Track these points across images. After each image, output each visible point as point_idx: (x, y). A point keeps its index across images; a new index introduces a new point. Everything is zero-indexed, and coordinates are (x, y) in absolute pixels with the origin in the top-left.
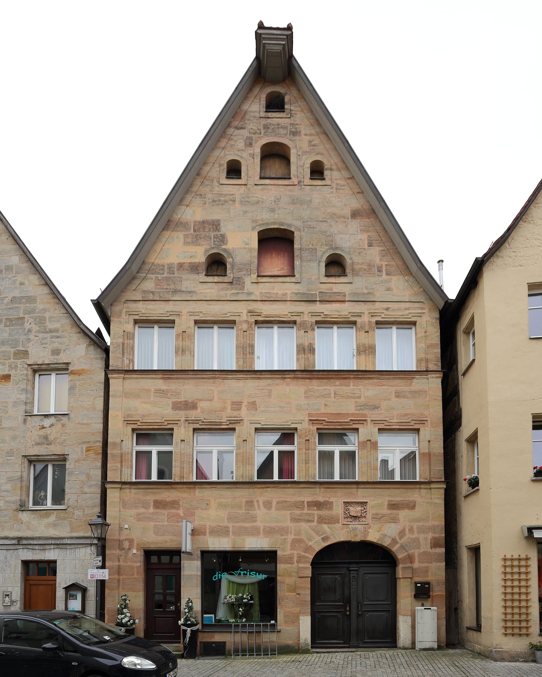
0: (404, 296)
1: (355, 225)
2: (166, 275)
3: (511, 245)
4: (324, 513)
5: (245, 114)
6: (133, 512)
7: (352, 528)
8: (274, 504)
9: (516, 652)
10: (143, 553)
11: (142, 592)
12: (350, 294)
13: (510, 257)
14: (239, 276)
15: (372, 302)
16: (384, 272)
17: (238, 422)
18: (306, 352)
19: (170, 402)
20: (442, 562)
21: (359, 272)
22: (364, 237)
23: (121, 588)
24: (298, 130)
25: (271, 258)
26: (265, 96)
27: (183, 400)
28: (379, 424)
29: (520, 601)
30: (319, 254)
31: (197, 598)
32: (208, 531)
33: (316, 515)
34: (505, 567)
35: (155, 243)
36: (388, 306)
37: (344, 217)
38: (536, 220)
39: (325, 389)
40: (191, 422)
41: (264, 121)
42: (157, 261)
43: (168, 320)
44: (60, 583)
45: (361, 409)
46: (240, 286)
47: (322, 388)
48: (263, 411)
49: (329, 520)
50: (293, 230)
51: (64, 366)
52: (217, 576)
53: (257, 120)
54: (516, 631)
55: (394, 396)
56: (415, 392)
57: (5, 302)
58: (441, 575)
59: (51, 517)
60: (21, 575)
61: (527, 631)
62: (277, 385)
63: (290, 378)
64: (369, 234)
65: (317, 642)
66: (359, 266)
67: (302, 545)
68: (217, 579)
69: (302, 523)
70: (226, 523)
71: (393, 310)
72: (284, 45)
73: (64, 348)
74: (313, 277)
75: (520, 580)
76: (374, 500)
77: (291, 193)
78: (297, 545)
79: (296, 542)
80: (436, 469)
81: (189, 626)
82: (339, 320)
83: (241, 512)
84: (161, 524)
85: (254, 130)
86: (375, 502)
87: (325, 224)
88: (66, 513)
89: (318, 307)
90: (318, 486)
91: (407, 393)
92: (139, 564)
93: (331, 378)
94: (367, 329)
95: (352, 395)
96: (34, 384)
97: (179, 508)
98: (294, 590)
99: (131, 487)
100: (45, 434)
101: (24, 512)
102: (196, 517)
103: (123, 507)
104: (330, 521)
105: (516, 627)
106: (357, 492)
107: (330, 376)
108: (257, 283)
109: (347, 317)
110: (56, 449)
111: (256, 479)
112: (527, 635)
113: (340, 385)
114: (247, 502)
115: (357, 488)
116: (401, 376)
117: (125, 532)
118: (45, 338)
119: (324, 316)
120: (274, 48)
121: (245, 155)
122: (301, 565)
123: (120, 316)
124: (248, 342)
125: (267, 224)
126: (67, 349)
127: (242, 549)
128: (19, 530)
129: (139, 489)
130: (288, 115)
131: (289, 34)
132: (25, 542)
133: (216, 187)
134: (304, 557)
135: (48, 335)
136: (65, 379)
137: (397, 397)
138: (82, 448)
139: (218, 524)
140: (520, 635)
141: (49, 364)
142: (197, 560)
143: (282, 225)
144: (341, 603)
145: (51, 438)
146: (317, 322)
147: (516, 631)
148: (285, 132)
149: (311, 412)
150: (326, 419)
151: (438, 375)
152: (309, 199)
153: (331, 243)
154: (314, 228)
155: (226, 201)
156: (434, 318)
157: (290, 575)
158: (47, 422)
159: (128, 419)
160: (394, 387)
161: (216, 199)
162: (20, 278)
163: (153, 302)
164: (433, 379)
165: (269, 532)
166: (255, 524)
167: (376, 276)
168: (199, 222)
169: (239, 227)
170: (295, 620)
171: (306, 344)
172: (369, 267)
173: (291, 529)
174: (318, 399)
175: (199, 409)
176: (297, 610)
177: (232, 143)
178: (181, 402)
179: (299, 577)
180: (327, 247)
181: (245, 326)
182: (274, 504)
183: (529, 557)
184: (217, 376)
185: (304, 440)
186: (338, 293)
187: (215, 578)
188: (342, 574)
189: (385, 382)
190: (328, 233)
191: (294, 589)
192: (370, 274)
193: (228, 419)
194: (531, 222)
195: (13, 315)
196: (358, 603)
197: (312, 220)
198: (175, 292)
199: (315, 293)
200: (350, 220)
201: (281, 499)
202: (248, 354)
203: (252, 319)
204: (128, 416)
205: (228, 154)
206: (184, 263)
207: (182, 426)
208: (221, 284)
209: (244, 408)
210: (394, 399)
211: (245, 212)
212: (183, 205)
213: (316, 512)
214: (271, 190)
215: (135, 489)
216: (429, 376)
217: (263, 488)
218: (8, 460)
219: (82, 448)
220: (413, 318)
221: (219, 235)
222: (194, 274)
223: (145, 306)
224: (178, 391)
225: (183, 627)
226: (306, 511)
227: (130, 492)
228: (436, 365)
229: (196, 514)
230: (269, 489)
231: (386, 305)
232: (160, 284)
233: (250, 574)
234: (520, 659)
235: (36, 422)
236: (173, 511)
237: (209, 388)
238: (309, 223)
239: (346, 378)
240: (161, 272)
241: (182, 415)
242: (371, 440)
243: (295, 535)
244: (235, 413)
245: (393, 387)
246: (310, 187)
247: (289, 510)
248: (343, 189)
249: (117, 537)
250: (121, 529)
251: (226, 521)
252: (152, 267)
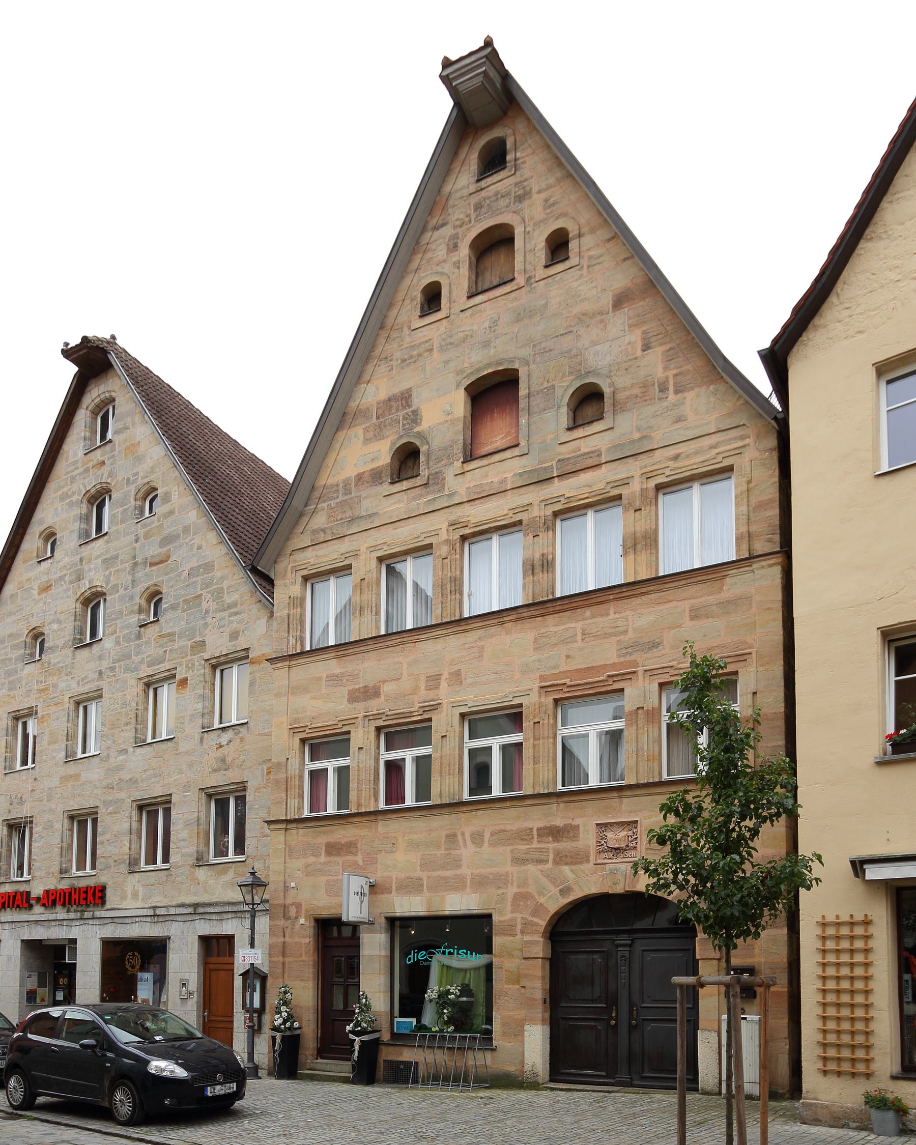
0: (708, 423)
1: (619, 320)
2: (341, 498)
3: (841, 297)
4: (565, 845)
5: (447, 199)
6: (299, 863)
7: (610, 869)
8: (487, 836)
9: (842, 1108)
10: (313, 924)
11: (311, 982)
12: (609, 449)
13: (839, 322)
14: (437, 470)
15: (648, 453)
16: (671, 389)
17: (435, 707)
18: (536, 571)
19: (345, 691)
20: (781, 927)
21: (626, 402)
22: (636, 337)
23: (286, 975)
24: (528, 189)
25: (492, 421)
26: (476, 155)
27: (362, 685)
28: (659, 676)
29: (852, 1006)
30: (559, 392)
31: (380, 992)
32: (394, 887)
33: (551, 851)
34: (824, 938)
35: (327, 454)
36: (677, 451)
37: (601, 313)
38: (891, 229)
39: (567, 629)
40: (371, 718)
41: (474, 199)
42: (332, 481)
43: (344, 566)
44: (238, 968)
45: (627, 653)
46: (439, 486)
47: (562, 627)
48: (470, 684)
49: (572, 857)
50: (516, 367)
51: (243, 654)
52: (411, 956)
53: (465, 201)
54: (846, 1067)
55: (688, 618)
56: (728, 602)
57: (182, 578)
58: (778, 954)
59: (229, 873)
60: (199, 957)
61: (868, 1067)
62: (492, 636)
63: (511, 621)
64: (644, 328)
65: (562, 1071)
66: (627, 393)
67: (529, 902)
68: (412, 961)
69: (529, 865)
70: (418, 873)
71: (688, 456)
72: (485, 72)
73: (243, 628)
74: (550, 437)
75: (852, 965)
76: (650, 817)
77: (515, 304)
78: (522, 903)
79: (521, 898)
80: (769, 745)
81: (358, 1034)
82: (590, 500)
83: (439, 853)
84: (335, 878)
85: (461, 219)
86: (652, 819)
87: (570, 337)
88: (245, 866)
89: (559, 488)
90: (554, 800)
91: (714, 608)
92: (307, 940)
93: (576, 608)
94: (637, 504)
95: (613, 630)
96: (214, 685)
97: (357, 852)
98: (517, 981)
99: (299, 825)
100: (221, 756)
101: (201, 868)
102: (379, 866)
103: (290, 856)
104: (574, 860)
105: (846, 1059)
106: (621, 803)
107: (574, 605)
108: (463, 473)
109: (604, 491)
110: (234, 776)
111: (466, 796)
112: (868, 1076)
113: (593, 616)
114: (448, 836)
115: (620, 797)
116: (699, 578)
117: (292, 893)
118: (223, 619)
119: (566, 501)
120: (468, 86)
121: (447, 268)
122: (527, 938)
123: (285, 576)
124: (449, 575)
125: (478, 370)
126: (246, 628)
127: (441, 913)
128: (195, 894)
129: (308, 828)
130: (510, 171)
131: (489, 53)
132: (201, 910)
133: (407, 337)
134: (532, 924)
135: (226, 614)
136: (247, 669)
137: (692, 618)
138: (263, 770)
139: (407, 874)
140: (854, 1075)
141: (227, 655)
142: (380, 933)
143: (501, 364)
144: (602, 1003)
145: (229, 759)
146: (556, 514)
147: (846, 1067)
148: (508, 201)
149: (543, 674)
150: (568, 681)
151: (772, 562)
152: (543, 302)
153: (578, 368)
154: (551, 350)
155: (420, 355)
156: (766, 451)
157: (511, 956)
158: (225, 737)
159: (295, 726)
160: (689, 601)
161: (406, 357)
162: (197, 541)
163: (325, 545)
164: (764, 570)
165: (480, 883)
166: (459, 872)
167: (657, 401)
168: (384, 401)
169: (437, 390)
170: (517, 1032)
171: (537, 556)
172: (644, 390)
173: (512, 876)
174: (556, 649)
175: (382, 696)
176: (522, 1013)
177: (429, 255)
178: (359, 688)
179: (524, 959)
180: (572, 377)
181: (444, 550)
182: (487, 836)
183: (870, 918)
184: (405, 640)
185: (532, 723)
186: (589, 453)
187: (410, 960)
188: (604, 952)
189: (670, 595)
190: (574, 352)
191: (517, 978)
192: (646, 400)
193: (421, 705)
194: (884, 236)
195: (191, 594)
196: (631, 1005)
197: (548, 338)
198: (352, 520)
199: (550, 464)
200: (611, 314)
201: (497, 828)
202: (449, 594)
203: (456, 536)
204: (296, 720)
205: (424, 277)
206: (364, 473)
207: (360, 727)
208: (412, 490)
209: (444, 684)
210: (688, 623)
211: (446, 362)
212: (362, 384)
213: (551, 846)
214: (485, 310)
215: (303, 828)
216: (754, 566)
217: (471, 811)
218: (185, 796)
219: (263, 770)
220: (724, 460)
221: (410, 413)
222: (376, 485)
223: (314, 553)
224: (356, 672)
225: (351, 1036)
226: (535, 845)
227: (298, 833)
228: (770, 540)
229: (379, 861)
230: (479, 813)
231: (672, 451)
232: (333, 514)
233: (458, 954)
234: (851, 1124)
235: (212, 739)
236: (351, 858)
237: (396, 660)
238: (543, 345)
239: (601, 603)
240: (335, 495)
241: (360, 709)
242: (643, 708)
243: (519, 886)
244: (432, 694)
245: (686, 602)
246: (545, 281)
247: (510, 844)
248: (599, 263)
249: (281, 902)
250: (286, 888)
251: (419, 868)
252: (324, 491)
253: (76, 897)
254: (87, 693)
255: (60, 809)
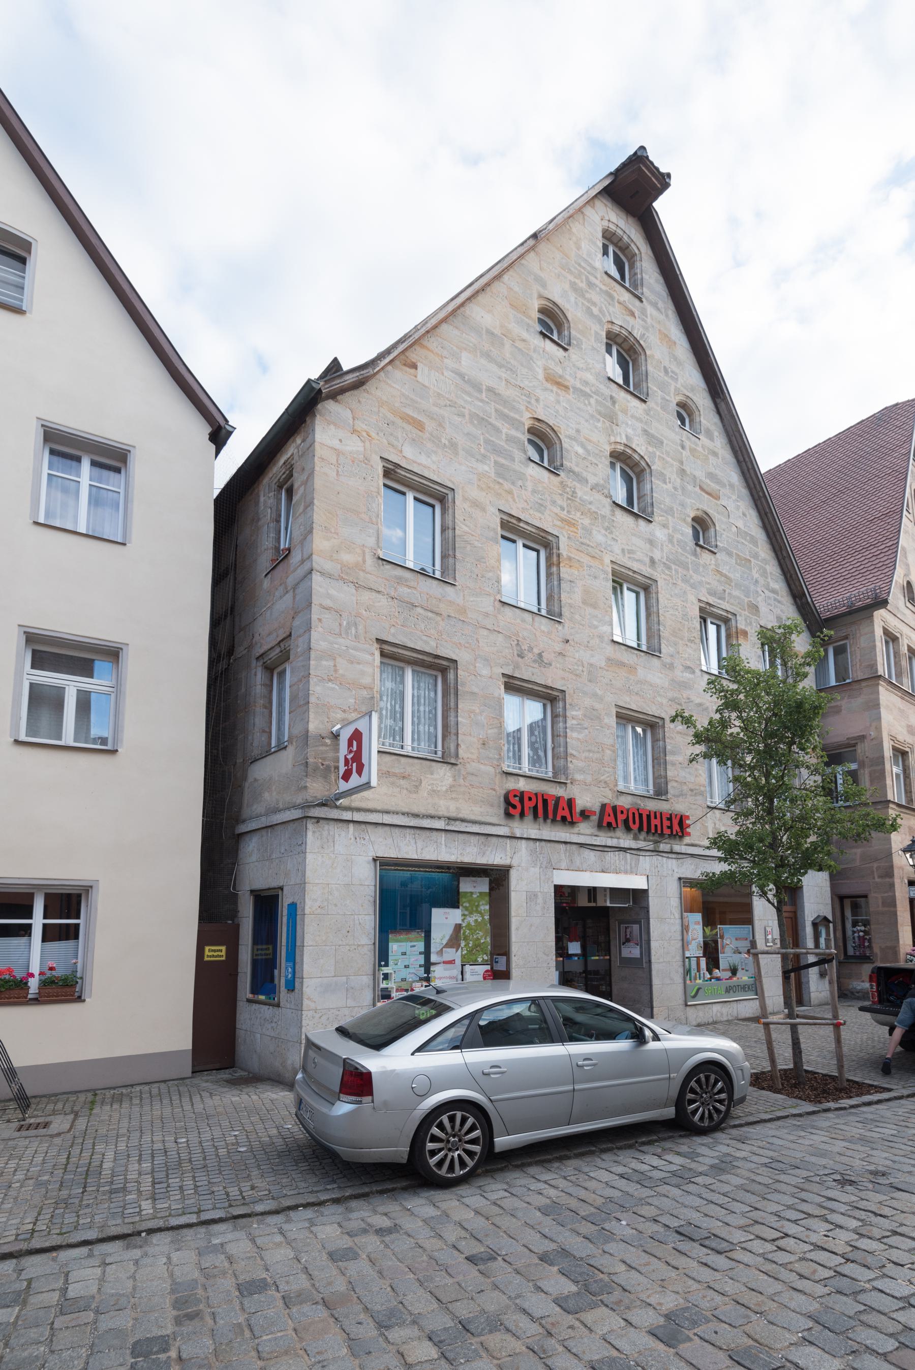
253: (658, 822)
254: (634, 572)
255: (611, 699)
